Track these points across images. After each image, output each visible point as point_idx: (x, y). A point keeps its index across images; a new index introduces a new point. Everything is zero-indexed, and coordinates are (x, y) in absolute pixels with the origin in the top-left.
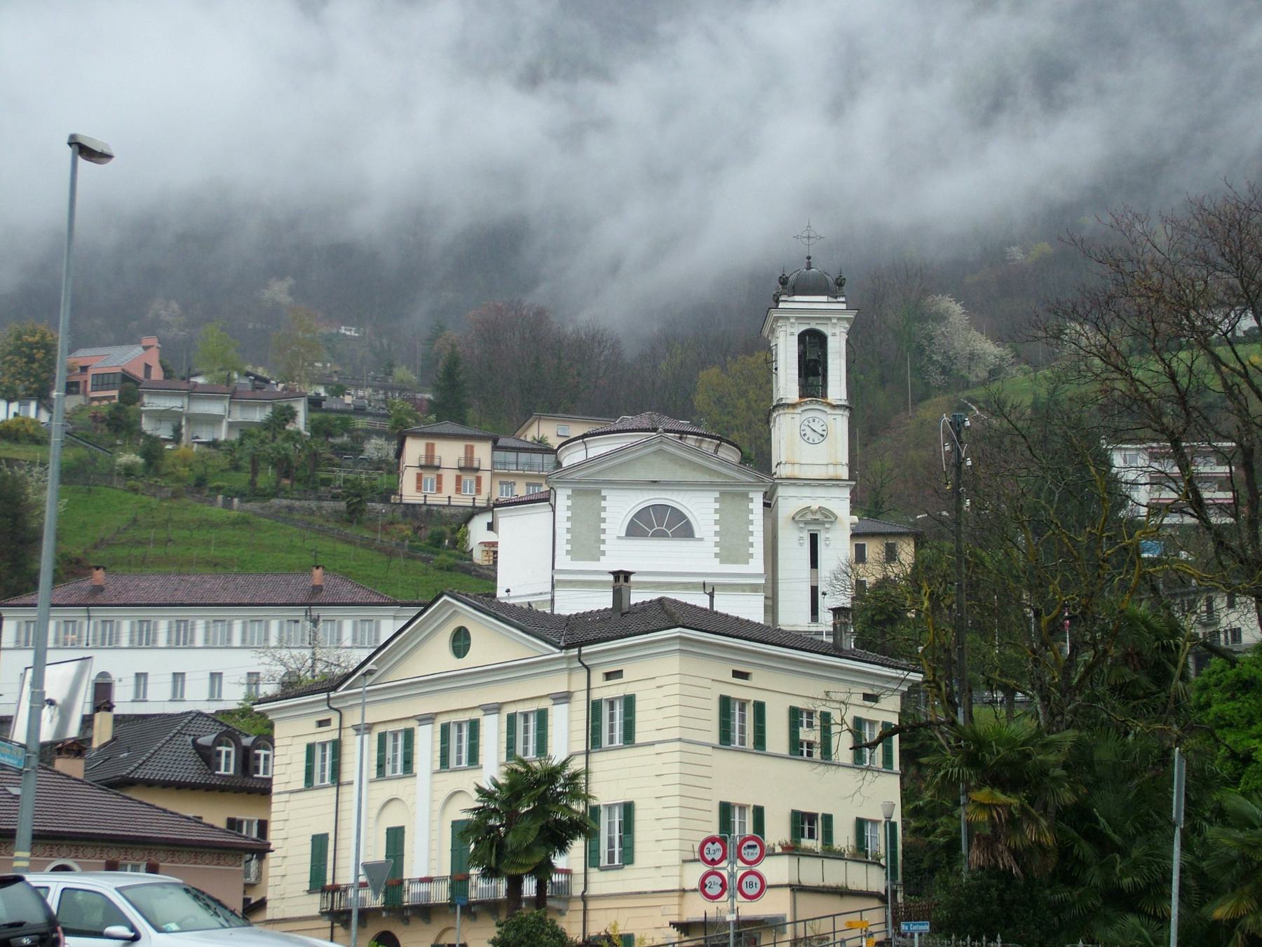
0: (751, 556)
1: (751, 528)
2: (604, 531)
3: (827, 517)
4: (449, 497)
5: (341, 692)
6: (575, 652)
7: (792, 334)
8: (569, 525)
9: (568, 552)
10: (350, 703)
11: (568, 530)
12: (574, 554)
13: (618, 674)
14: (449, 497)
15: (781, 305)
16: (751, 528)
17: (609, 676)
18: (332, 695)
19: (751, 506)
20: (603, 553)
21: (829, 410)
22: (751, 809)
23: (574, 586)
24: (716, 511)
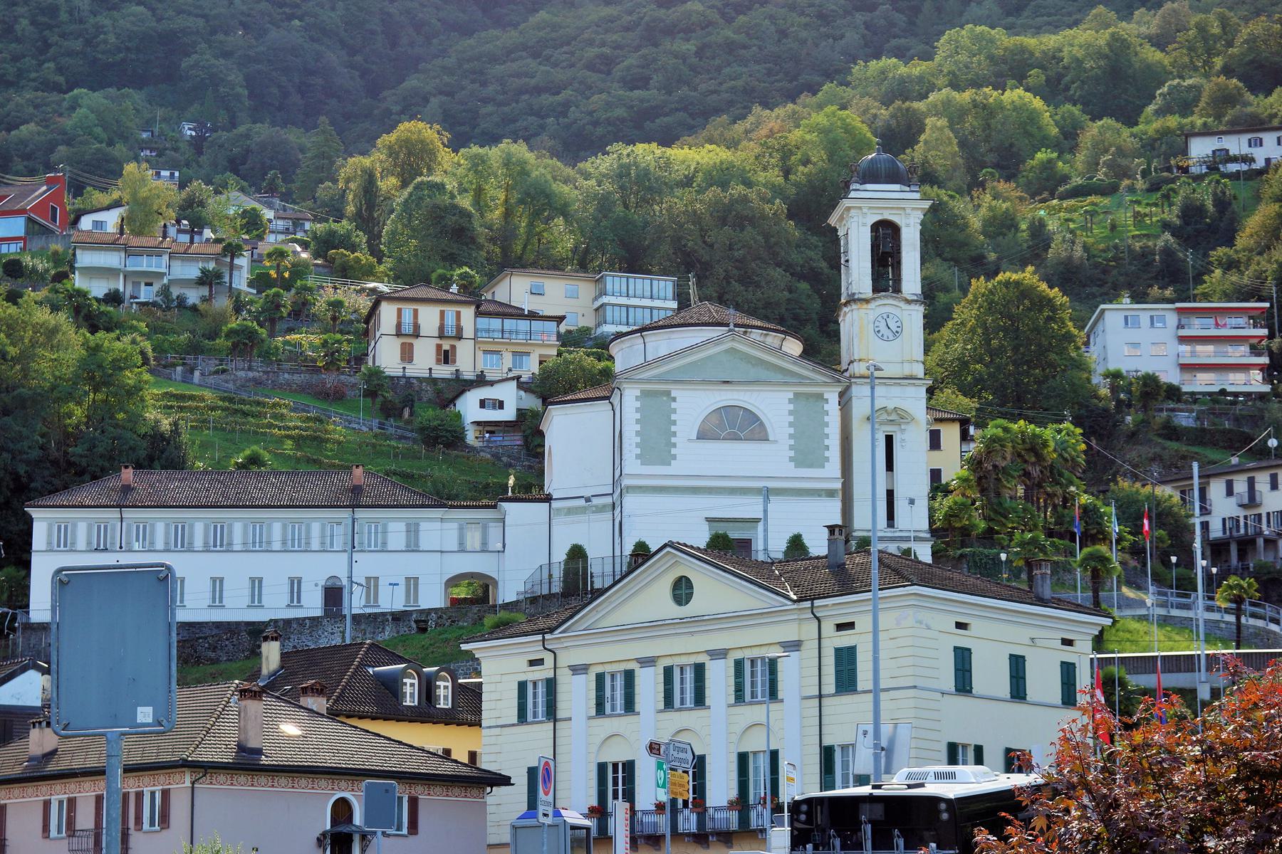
0: (827, 459)
1: (827, 430)
2: (674, 434)
3: (901, 417)
4: (430, 369)
5: (557, 634)
6: (808, 604)
7: (864, 225)
8: (638, 428)
9: (638, 457)
10: (565, 645)
11: (638, 433)
12: (644, 458)
13: (851, 625)
14: (430, 369)
15: (852, 194)
16: (827, 430)
17: (840, 627)
18: (547, 636)
19: (826, 407)
20: (674, 457)
21: (902, 304)
22: (973, 748)
23: (644, 492)
24: (791, 413)
